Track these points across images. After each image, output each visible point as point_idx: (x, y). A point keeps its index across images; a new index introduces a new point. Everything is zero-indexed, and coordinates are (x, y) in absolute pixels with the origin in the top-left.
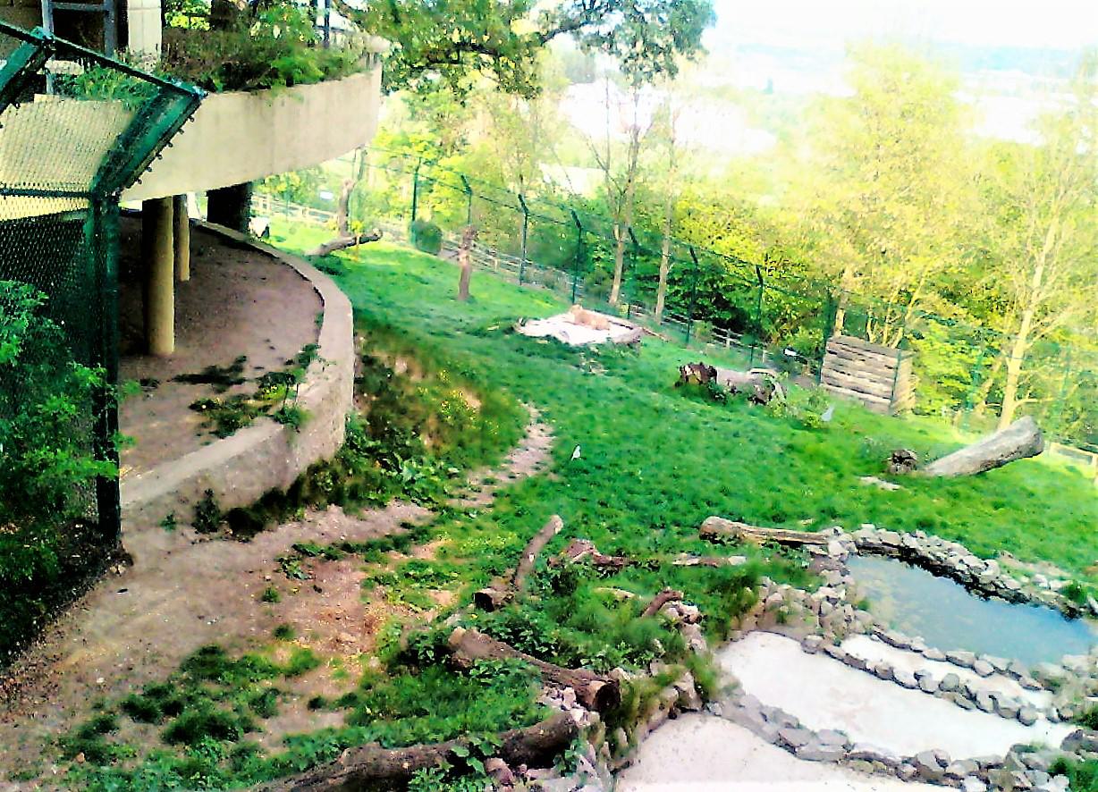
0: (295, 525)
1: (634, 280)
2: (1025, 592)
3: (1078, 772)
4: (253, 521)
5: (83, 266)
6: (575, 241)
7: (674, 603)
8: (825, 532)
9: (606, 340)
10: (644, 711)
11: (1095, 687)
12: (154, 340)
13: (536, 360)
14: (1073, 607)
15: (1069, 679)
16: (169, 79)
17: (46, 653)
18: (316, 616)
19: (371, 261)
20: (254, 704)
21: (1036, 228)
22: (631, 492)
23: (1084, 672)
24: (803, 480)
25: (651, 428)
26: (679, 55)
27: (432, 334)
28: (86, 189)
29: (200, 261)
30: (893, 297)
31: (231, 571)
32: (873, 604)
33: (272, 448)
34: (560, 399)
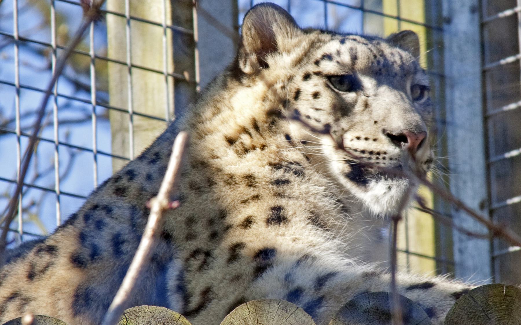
0: (8, 313)
1: (284, 192)
2: (261, 129)
3: (212, 300)
4: (167, 131)
5: (107, 197)
6: (324, 80)
7: (179, 248)
8: (294, 271)
9: (246, 157)
10: (234, 207)
11: (1, 288)
12: (381, 87)
13: (87, 246)
14: (164, 323)
15: (176, 283)
16: (38, 283)
17: (141, 312)
18: (369, 303)
19: (449, 273)
20: (273, 209)
21: (300, 212)
22: (405, 116)
23: (272, 90)
24: (144, 317)
25: (244, 202)
26: (155, 149)
27: (317, 110)
28: (393, 224)
29: (218, 303)
30: (224, 88)
31: (395, 131)
32: (301, 215)
33: (64, 296)
34: (117, 219)
